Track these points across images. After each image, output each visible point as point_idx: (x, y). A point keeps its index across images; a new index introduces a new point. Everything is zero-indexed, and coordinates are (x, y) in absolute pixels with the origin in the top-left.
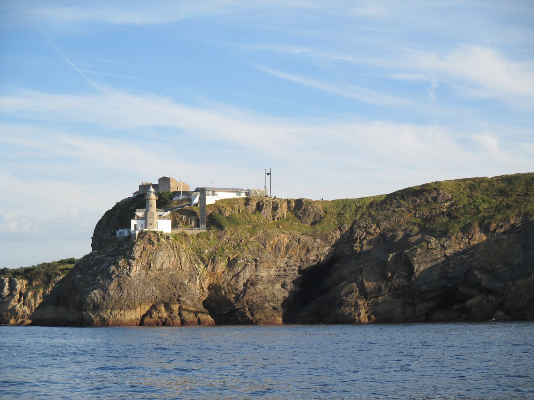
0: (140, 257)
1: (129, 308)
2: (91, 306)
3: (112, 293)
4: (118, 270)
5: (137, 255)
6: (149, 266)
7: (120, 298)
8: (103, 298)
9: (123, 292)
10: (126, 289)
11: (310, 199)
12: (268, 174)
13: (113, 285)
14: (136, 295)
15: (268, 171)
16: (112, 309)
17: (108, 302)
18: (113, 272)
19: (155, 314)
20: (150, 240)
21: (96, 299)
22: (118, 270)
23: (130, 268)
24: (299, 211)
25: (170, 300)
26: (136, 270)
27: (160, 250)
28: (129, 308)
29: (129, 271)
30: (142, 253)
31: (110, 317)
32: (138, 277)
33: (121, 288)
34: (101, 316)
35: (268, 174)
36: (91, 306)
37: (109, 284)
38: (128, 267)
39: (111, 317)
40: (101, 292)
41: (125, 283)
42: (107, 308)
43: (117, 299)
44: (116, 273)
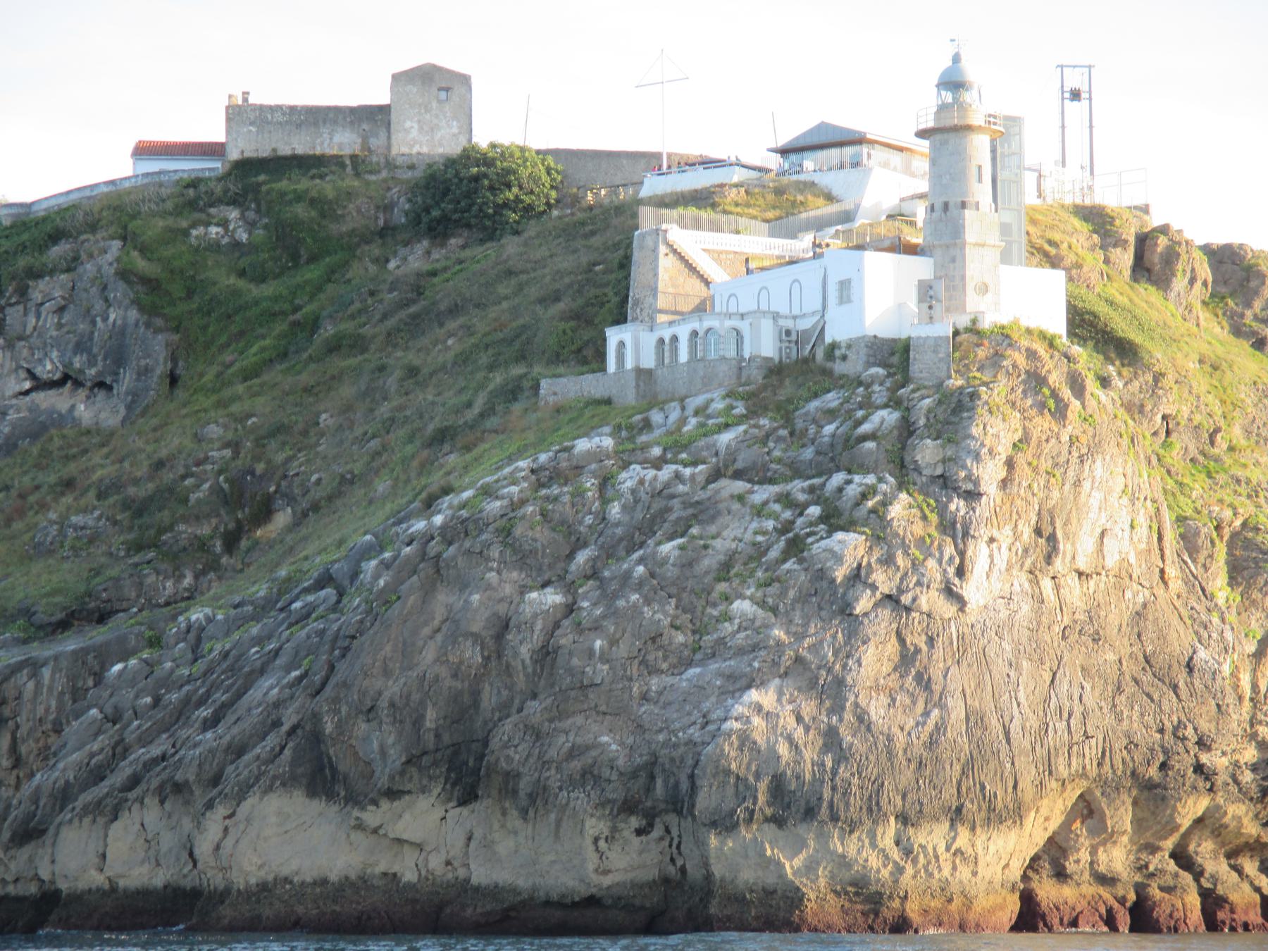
0: (1004, 483)
1: (991, 809)
2: (762, 798)
3: (877, 710)
4: (888, 561)
5: (989, 474)
6: (1048, 540)
7: (932, 743)
8: (831, 740)
9: (941, 705)
10: (957, 683)
11: (1224, 242)
12: (1076, 95)
13: (874, 660)
14: (1015, 728)
15: (1075, 80)
16: (903, 819)
17: (872, 771)
18: (858, 576)
19: (1079, 861)
20: (1036, 381)
21: (783, 749)
22: (888, 561)
23: (962, 554)
24: (1249, 305)
25: (1163, 766)
26: (992, 575)
27: (1094, 449)
28: (991, 809)
29: (960, 572)
30: (1010, 464)
31: (900, 870)
32: (1004, 614)
33: (924, 682)
34: (843, 862)
35: (1076, 95)
36: (762, 798)
37: (847, 651)
38: (949, 550)
39: (910, 871)
40: (808, 708)
41: (938, 653)
42: (874, 810)
43: (918, 750)
44: (884, 581)
